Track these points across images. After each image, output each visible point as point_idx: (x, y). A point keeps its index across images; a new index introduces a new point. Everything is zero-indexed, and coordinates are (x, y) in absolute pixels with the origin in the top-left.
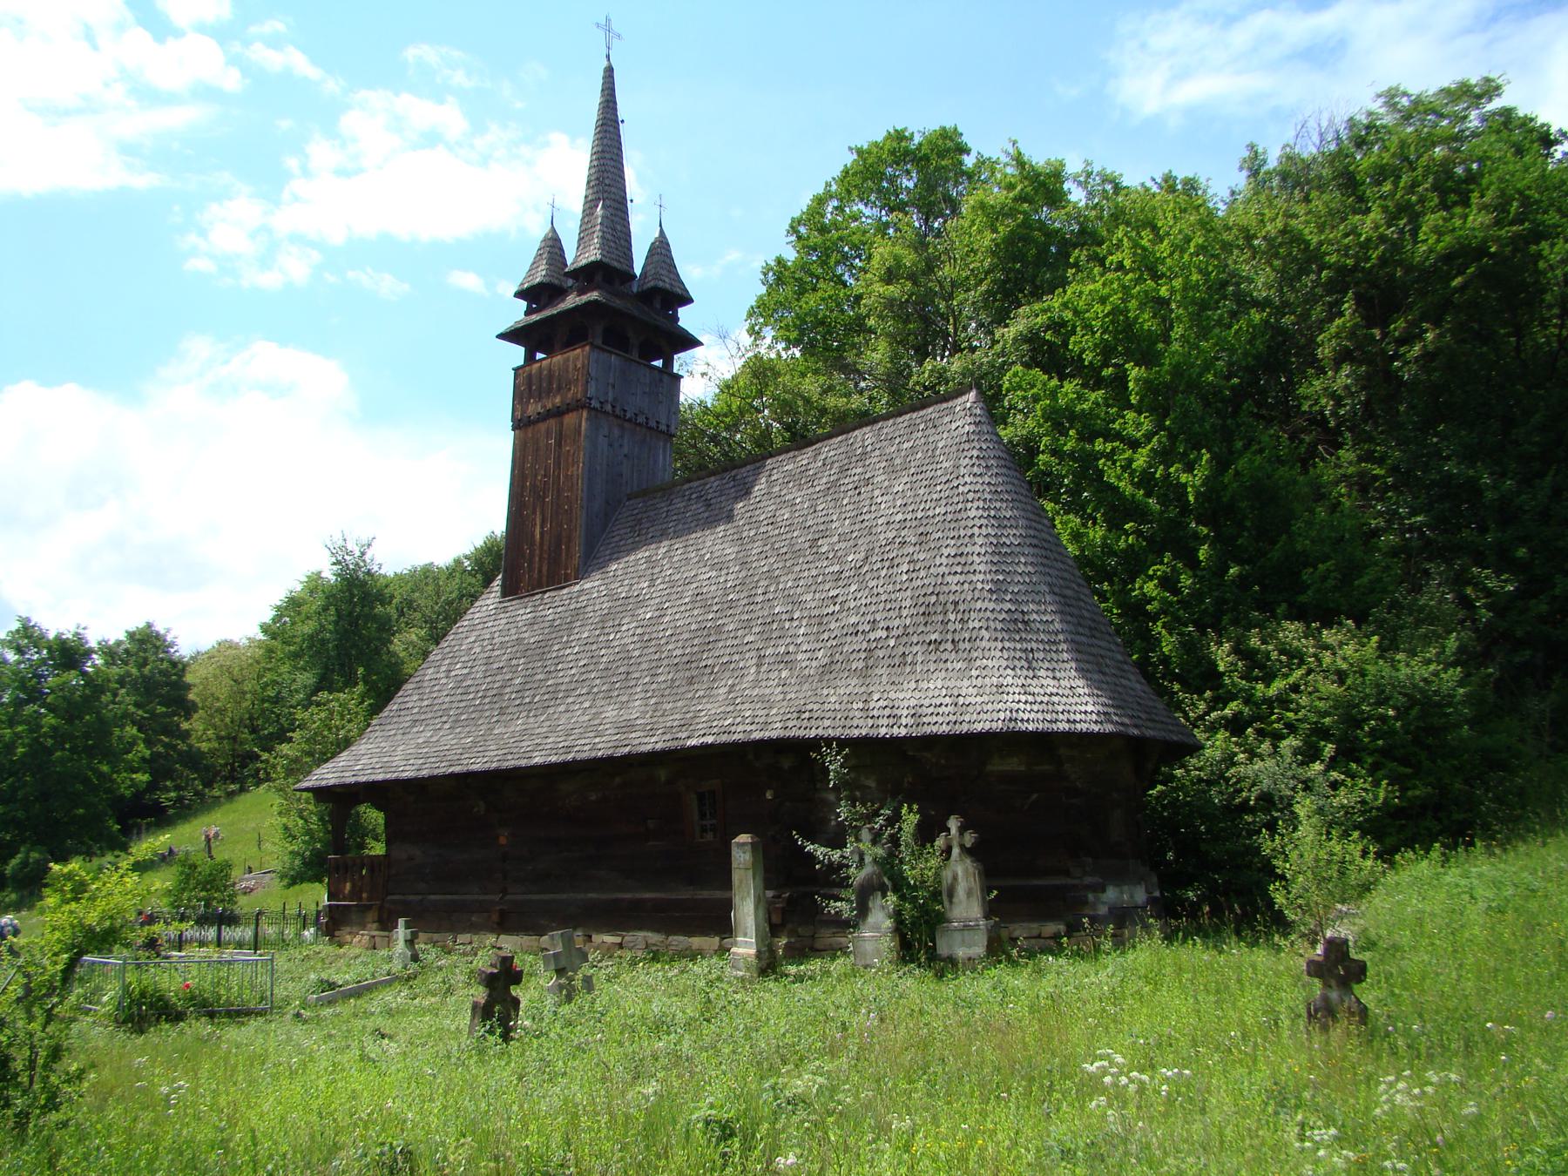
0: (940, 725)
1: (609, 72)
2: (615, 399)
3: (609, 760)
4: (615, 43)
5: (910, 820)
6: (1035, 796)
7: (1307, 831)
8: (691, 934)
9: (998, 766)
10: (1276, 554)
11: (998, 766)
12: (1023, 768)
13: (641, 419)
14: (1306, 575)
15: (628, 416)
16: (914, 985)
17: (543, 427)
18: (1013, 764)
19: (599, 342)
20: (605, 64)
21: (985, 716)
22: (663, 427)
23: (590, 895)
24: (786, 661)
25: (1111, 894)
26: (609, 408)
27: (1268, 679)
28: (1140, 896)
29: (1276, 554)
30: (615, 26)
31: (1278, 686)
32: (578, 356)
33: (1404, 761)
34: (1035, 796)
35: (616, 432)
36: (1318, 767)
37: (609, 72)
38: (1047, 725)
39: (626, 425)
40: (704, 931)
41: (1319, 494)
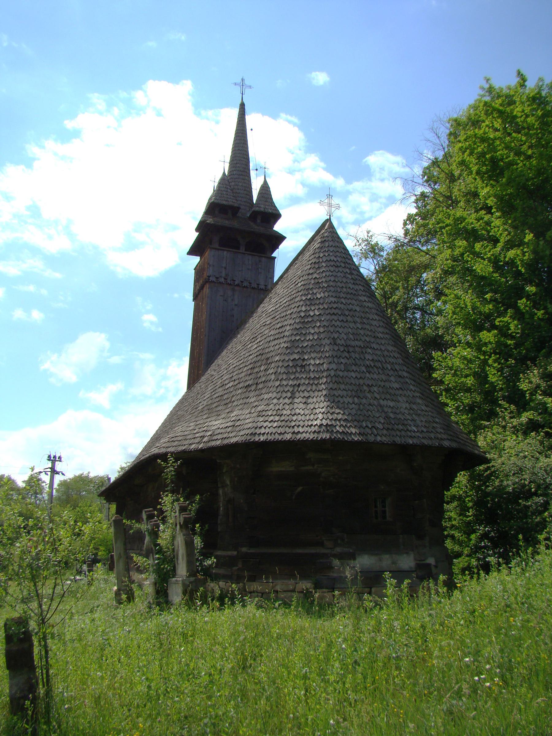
2: (227, 275)
4: (247, 91)
6: (300, 489)
12: (292, 469)
13: (245, 284)
15: (236, 283)
18: (283, 467)
19: (216, 246)
20: (240, 102)
21: (269, 430)
22: (262, 287)
23: (221, 509)
26: (222, 280)
30: (247, 82)
34: (300, 489)
35: (230, 293)
37: (242, 107)
38: (316, 435)
39: (236, 288)
41: (522, 161)
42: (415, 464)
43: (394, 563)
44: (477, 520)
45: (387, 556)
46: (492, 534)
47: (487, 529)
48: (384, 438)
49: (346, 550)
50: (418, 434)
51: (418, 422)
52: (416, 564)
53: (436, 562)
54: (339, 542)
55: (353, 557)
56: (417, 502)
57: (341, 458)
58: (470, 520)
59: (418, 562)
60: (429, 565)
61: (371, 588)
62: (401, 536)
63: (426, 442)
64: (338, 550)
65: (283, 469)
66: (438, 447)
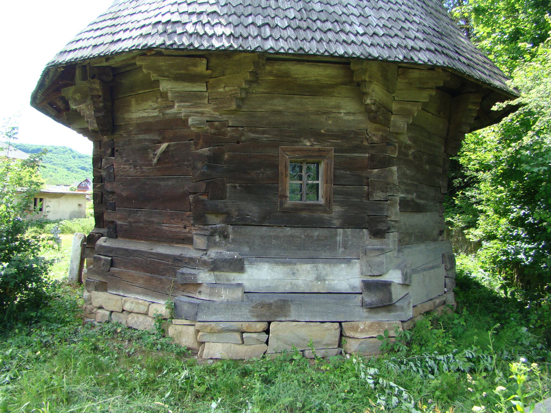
6: (164, 146)
34: (164, 146)
42: (368, 102)
43: (319, 278)
44: (513, 196)
45: (308, 267)
46: (531, 220)
47: (523, 211)
48: (282, 43)
49: (227, 254)
50: (365, 39)
51: (373, 21)
52: (363, 281)
53: (405, 276)
54: (217, 238)
55: (238, 266)
56: (376, 170)
57: (221, 90)
58: (502, 196)
59: (366, 279)
60: (387, 285)
61: (269, 323)
62: (340, 231)
63: (375, 52)
64: (213, 253)
65: (145, 115)
66: (402, 62)
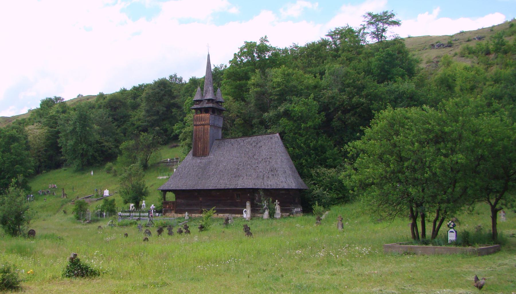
0: (274, 187)
1: (209, 56)
3: (224, 189)
5: (271, 200)
7: (317, 206)
8: (236, 214)
9: (281, 192)
10: (323, 157)
11: (281, 192)
14: (328, 161)
16: (170, 237)
17: (200, 127)
18: (283, 192)
24: (250, 176)
25: (296, 209)
27: (320, 177)
28: (299, 210)
29: (323, 157)
31: (321, 178)
32: (207, 115)
33: (339, 191)
36: (325, 192)
37: (209, 56)
40: (238, 213)
